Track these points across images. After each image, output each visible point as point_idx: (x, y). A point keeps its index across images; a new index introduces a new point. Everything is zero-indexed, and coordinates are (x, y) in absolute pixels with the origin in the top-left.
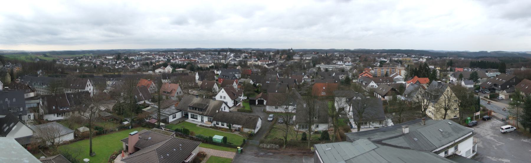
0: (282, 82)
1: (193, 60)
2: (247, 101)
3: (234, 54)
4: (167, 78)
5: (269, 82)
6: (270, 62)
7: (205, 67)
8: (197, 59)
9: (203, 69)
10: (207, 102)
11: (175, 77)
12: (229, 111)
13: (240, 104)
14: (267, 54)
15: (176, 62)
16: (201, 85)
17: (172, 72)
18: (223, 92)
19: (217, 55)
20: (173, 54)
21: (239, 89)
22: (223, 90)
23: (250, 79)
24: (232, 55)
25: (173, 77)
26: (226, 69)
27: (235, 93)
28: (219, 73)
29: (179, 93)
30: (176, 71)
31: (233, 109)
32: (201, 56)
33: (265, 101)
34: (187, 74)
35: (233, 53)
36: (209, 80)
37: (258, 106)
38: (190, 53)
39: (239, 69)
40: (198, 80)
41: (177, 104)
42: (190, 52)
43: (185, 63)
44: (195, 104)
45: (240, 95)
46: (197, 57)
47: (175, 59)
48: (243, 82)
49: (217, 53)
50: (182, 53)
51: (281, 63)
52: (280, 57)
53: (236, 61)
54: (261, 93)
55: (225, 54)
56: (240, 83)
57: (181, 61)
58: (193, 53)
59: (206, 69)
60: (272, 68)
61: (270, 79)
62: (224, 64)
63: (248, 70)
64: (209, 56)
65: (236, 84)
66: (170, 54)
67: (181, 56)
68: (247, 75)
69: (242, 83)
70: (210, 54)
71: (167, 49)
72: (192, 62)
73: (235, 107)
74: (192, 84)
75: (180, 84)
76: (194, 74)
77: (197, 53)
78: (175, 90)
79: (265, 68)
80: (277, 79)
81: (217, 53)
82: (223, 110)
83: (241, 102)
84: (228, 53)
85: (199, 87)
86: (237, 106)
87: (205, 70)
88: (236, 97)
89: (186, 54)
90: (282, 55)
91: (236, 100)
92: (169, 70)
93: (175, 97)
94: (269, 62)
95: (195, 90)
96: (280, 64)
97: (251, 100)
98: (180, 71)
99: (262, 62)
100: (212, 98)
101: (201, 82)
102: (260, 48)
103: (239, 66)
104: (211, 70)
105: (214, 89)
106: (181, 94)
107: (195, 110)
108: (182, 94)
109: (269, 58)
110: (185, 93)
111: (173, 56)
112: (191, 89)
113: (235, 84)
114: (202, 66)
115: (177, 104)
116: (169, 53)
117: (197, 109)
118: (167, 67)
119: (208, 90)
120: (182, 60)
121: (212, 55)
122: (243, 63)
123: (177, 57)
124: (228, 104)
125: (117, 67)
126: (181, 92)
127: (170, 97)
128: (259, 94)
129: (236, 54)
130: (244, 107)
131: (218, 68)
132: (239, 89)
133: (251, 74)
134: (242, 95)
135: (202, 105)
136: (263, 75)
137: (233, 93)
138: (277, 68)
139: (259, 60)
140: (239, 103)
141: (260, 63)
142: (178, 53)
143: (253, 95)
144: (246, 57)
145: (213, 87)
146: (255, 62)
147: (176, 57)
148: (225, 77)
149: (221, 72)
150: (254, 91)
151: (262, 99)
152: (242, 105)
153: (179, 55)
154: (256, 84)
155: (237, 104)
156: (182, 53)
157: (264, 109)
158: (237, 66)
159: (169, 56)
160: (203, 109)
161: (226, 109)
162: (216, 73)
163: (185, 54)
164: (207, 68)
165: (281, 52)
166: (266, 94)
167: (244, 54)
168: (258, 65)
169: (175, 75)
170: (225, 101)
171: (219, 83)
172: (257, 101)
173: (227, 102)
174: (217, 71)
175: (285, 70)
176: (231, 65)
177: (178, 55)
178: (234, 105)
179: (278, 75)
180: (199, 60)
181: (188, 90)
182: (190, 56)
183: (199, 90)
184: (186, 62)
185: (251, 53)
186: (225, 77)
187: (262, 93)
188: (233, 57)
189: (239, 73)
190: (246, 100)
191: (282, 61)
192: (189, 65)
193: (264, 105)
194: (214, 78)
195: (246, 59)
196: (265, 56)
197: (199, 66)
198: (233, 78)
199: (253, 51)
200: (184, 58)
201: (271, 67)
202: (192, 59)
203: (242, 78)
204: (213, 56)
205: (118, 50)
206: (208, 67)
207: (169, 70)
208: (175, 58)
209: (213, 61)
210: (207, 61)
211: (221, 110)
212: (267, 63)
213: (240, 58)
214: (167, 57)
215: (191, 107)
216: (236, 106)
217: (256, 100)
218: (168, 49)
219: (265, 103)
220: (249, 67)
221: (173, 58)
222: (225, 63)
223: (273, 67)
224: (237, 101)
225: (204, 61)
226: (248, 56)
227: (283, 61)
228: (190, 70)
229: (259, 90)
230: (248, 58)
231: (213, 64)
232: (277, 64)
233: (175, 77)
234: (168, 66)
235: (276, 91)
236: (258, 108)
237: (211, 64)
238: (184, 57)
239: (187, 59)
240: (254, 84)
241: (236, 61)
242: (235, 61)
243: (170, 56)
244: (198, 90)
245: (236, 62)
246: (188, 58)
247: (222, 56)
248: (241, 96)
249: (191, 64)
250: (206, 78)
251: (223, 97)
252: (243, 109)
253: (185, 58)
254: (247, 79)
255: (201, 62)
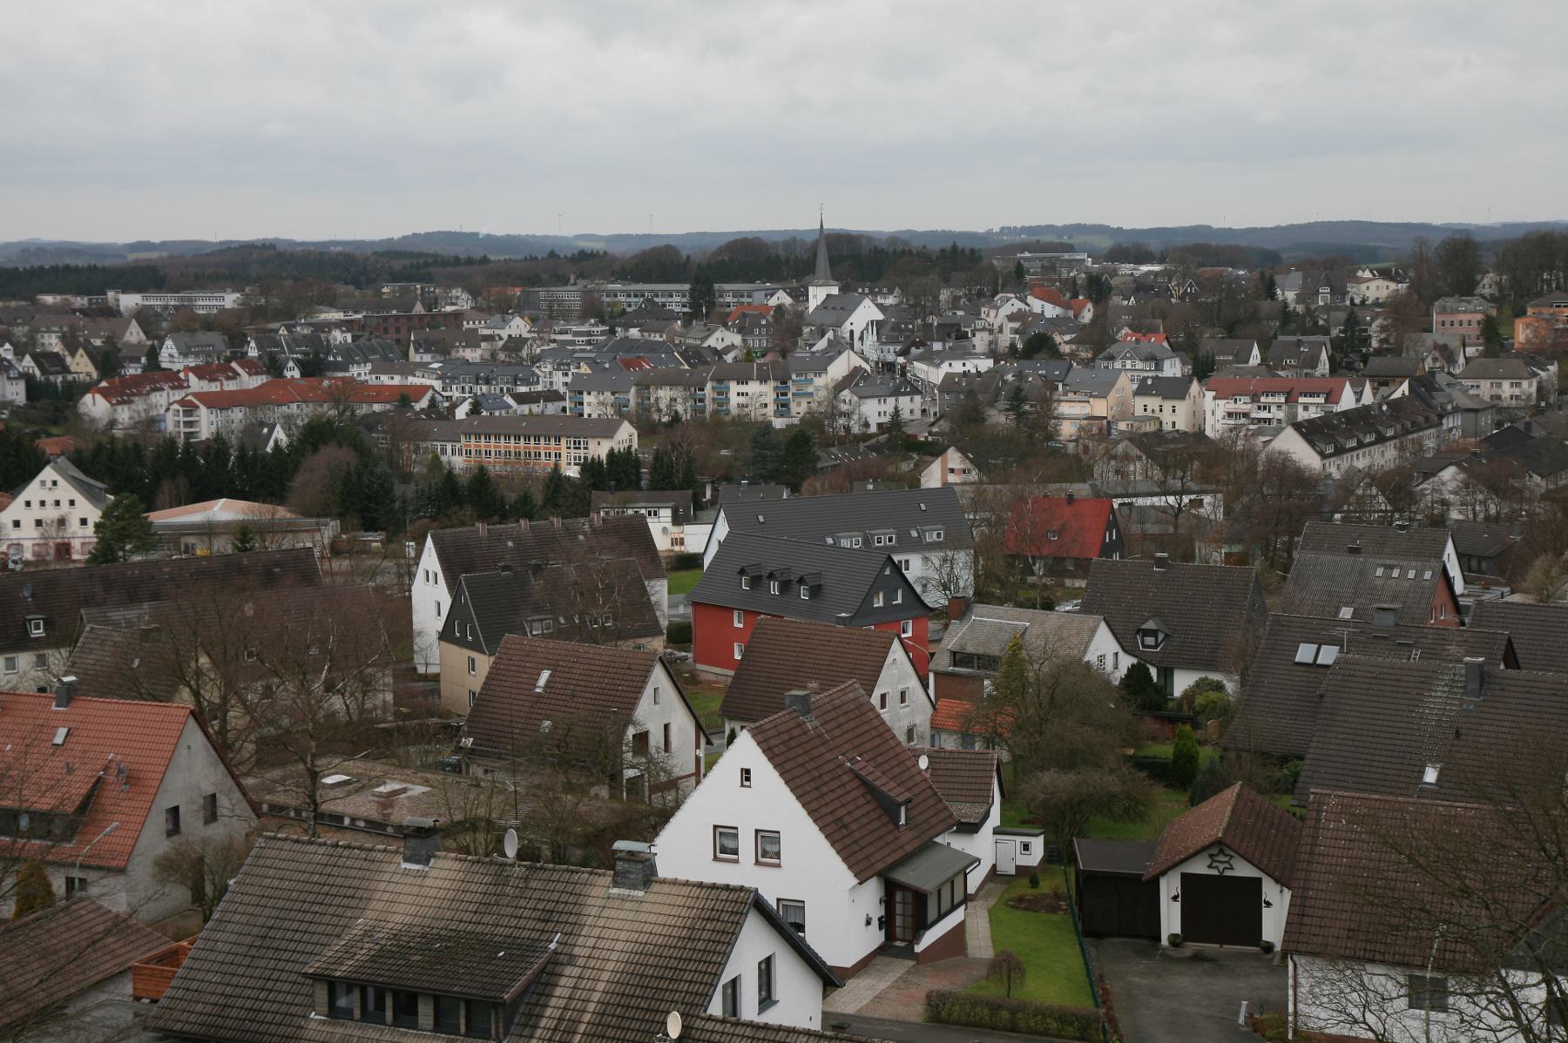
0: (1511, 660)
1: (380, 393)
2: (1046, 887)
3: (890, 301)
4: (38, 633)
5: (1329, 655)
6: (1347, 401)
7: (528, 477)
8: (426, 379)
9: (512, 497)
10: (547, 917)
11: (132, 614)
12: (816, 1026)
13: (959, 930)
14: (1306, 296)
15: (152, 422)
16: (481, 701)
17: (105, 552)
18: (746, 774)
19: (673, 316)
20: (112, 313)
21: (949, 743)
22: (745, 750)
23: (1086, 609)
24: (866, 313)
25: (116, 615)
26: (795, 488)
27: (898, 793)
28: (701, 538)
29: (192, 823)
30: (147, 538)
31: (878, 998)
32: (473, 340)
33: (1270, 890)
34: (301, 567)
35: (873, 294)
36: (577, 633)
37: (1179, 960)
38: (332, 303)
39: (947, 487)
40: (445, 635)
41: (161, 959)
42: (341, 289)
43: (279, 434)
44: (399, 947)
45: (964, 810)
46: (426, 346)
47: (136, 382)
48: (994, 649)
49: (676, 298)
50: (230, 300)
51: (1495, 405)
52: (1493, 336)
53: (913, 388)
54: (1227, 784)
55: (779, 308)
56: (959, 658)
57: (217, 402)
58: (380, 304)
59: (538, 498)
60: (1374, 478)
61: (1346, 613)
62: (767, 427)
63: (1071, 499)
64: (579, 333)
65: (913, 683)
66: (65, 310)
67: (216, 339)
68: (1057, 568)
69: (986, 662)
70: (583, 317)
71: (26, 249)
72: (362, 410)
73: (902, 966)
74: (367, 686)
75: (212, 694)
76: (388, 564)
77: (430, 304)
78: (131, 779)
79: (1285, 471)
80: (1446, 617)
81: (676, 298)
82: (749, 1009)
83: (967, 899)
84: (817, 295)
85: (452, 732)
86: (915, 957)
87: (525, 508)
88: (908, 840)
89: (287, 314)
90: (1515, 299)
91: (905, 876)
92: (62, 522)
93: (141, 870)
94: (1332, 396)
95: (404, 764)
96: (1486, 420)
97: (1089, 882)
98: (209, 530)
99: (1243, 405)
100: (609, 861)
101: (484, 662)
102: (1217, 223)
103: (954, 458)
104: (604, 511)
105: (642, 738)
106: (217, 831)
107: (397, 1023)
108: (234, 821)
109: (1337, 345)
110: (277, 810)
111: (110, 341)
112: (349, 755)
113: (897, 671)
114: (495, 467)
115: (173, 958)
116: (49, 299)
117: (425, 1012)
118: (33, 491)
119: (564, 764)
120: (230, 386)
121: (612, 318)
122: (998, 418)
123: (169, 353)
124: (813, 937)
125: (331, 359)
126: (223, 801)
127: (70, 882)
128: (1206, 807)
129: (918, 306)
130: (1006, 966)
131: (691, 483)
132: (949, 743)
133: (1106, 550)
134: (987, 815)
135: (481, 946)
136: (1258, 564)
137: (864, 783)
138: (1449, 474)
139: (1203, 370)
140: (941, 917)
141: (1224, 406)
142: (171, 300)
143: (1134, 810)
144: (1037, 345)
145: (629, 721)
146: (1153, 403)
147: (153, 354)
148: (785, 587)
149: (722, 529)
150: (1140, 764)
151: (1243, 870)
152: (981, 944)
153: (187, 324)
154: (1167, 674)
155: (921, 925)
156: (230, 300)
157: (1260, 1005)
158: (933, 450)
159: (53, 343)
160: (497, 1005)
161: (779, 991)
162: (662, 543)
163: (259, 314)
164: (556, 479)
165: (1499, 269)
166: (1286, 802)
167: (1013, 305)
168: (1200, 435)
169: (133, 590)
170: (772, 887)
171: (708, 672)
172: (1170, 887)
173: (799, 907)
174: (677, 520)
175: (1547, 497)
176: (849, 440)
177: (175, 330)
178: (890, 936)
179: (1454, 571)
180: (456, 394)
181: (314, 776)
182: (338, 336)
183: (457, 769)
184: (288, 422)
185: (1098, 289)
186: (774, 588)
187: (1231, 794)
188: (871, 338)
189: (953, 542)
190: (1034, 883)
191: (1515, 378)
192: (331, 456)
193: (1269, 948)
194: (645, 606)
195: (1036, 371)
196: (1286, 317)
197: (457, 460)
198: (879, 602)
199: (1126, 269)
200: (253, 368)
201: (1361, 462)
202: (361, 372)
203: (982, 596)
204: (634, 332)
205: (873, 232)
206: (573, 472)
207: (62, 522)
208: (133, 370)
209: (632, 396)
210: (553, 396)
211: (716, 1008)
212: (1310, 409)
213: (966, 354)
214: (20, 352)
215: (350, 984)
216: (908, 953)
217: (1154, 885)
218: (40, 249)
219: (1273, 926)
220: (1078, 468)
221: (108, 362)
222: (779, 423)
223: (1384, 457)
224: (928, 885)
225: (521, 399)
226: (1056, 322)
227: (1529, 387)
228: (341, 516)
229: (1206, 754)
230: (1054, 352)
231: (626, 436)
232: (1449, 423)
233: (140, 614)
234: (48, 473)
235: (1431, 776)
236: (1186, 983)
237: (605, 429)
238: (253, 352)
239: (293, 373)
240: (1137, 676)
241: (913, 388)
242: (896, 393)
243: (71, 345)
244: (441, 767)
245: (905, 403)
246: (312, 368)
247: (741, 330)
248: (972, 828)
249: (359, 448)
250: (537, 609)
251: (746, 845)
252: (994, 991)
253: (273, 366)
254: (1052, 619)
255: (475, 410)
